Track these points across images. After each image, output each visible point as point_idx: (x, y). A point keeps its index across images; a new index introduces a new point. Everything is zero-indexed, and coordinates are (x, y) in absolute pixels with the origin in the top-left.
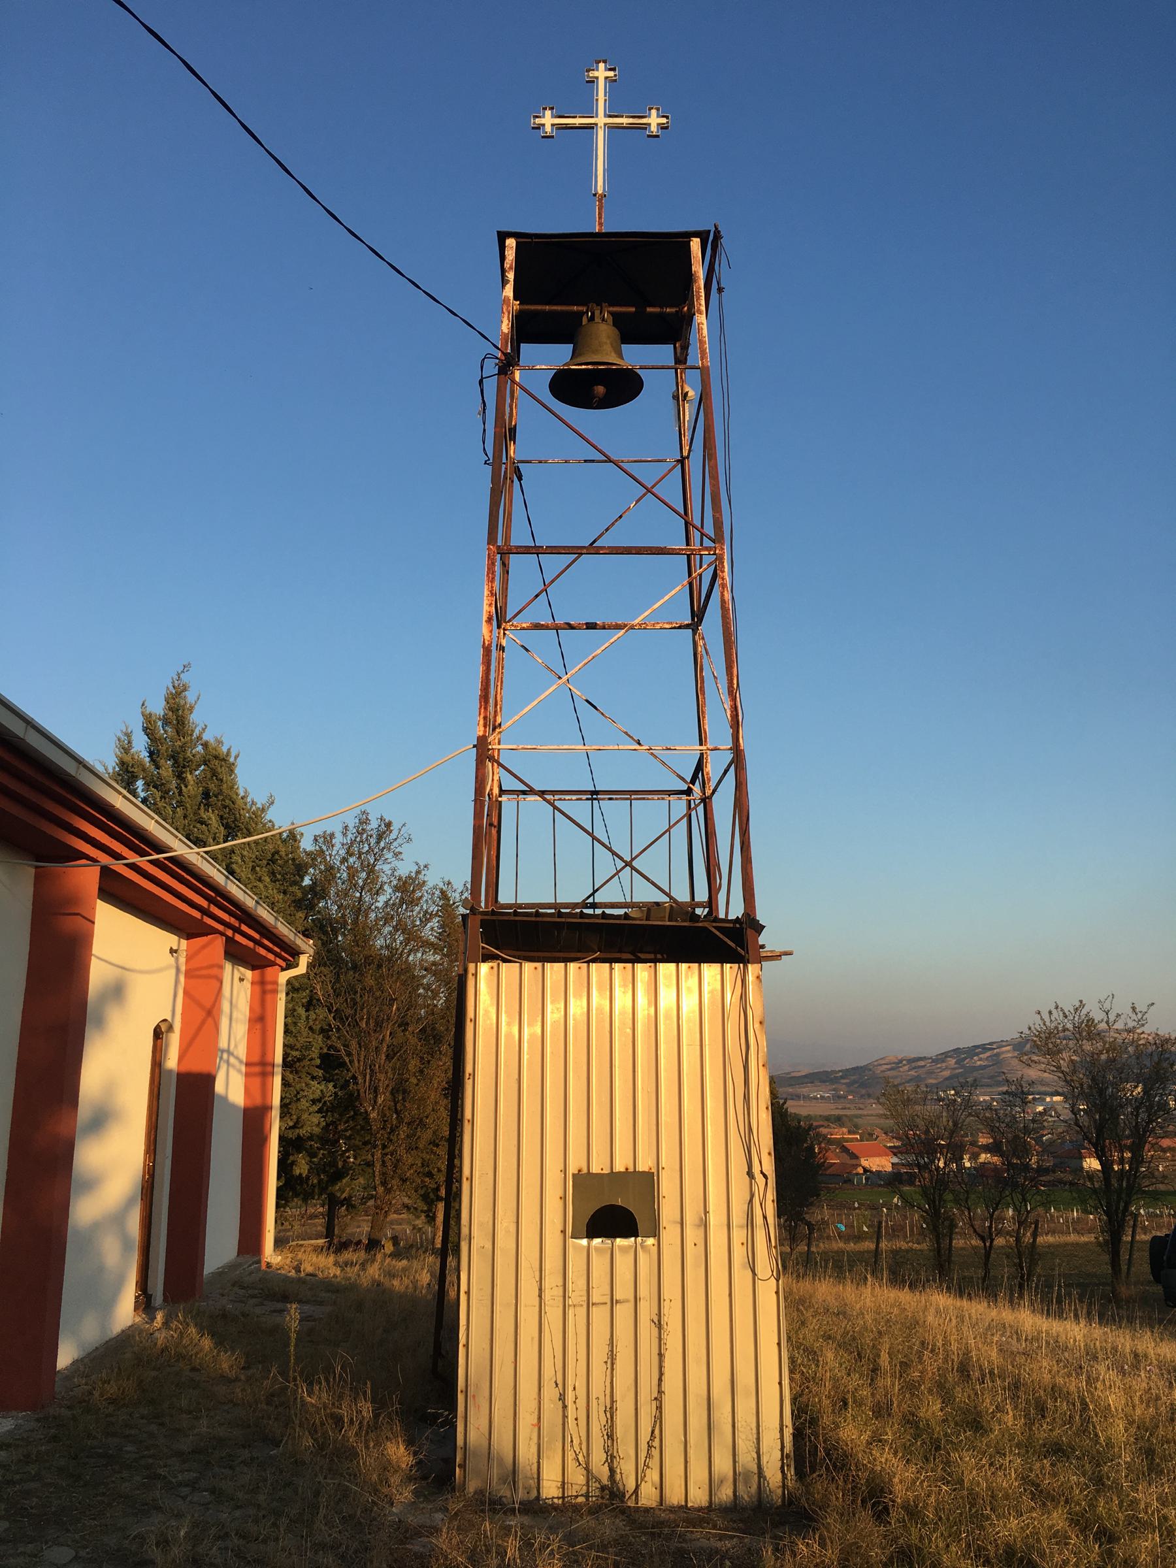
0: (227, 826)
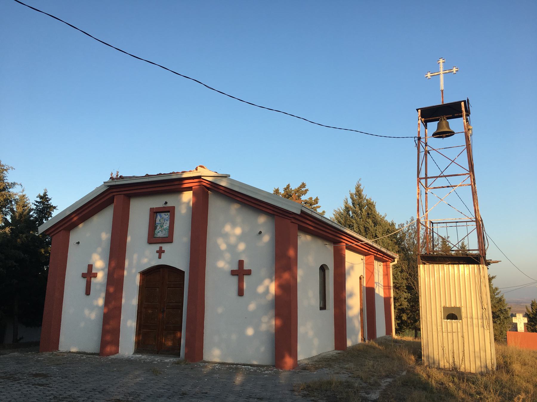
0: (374, 223)
